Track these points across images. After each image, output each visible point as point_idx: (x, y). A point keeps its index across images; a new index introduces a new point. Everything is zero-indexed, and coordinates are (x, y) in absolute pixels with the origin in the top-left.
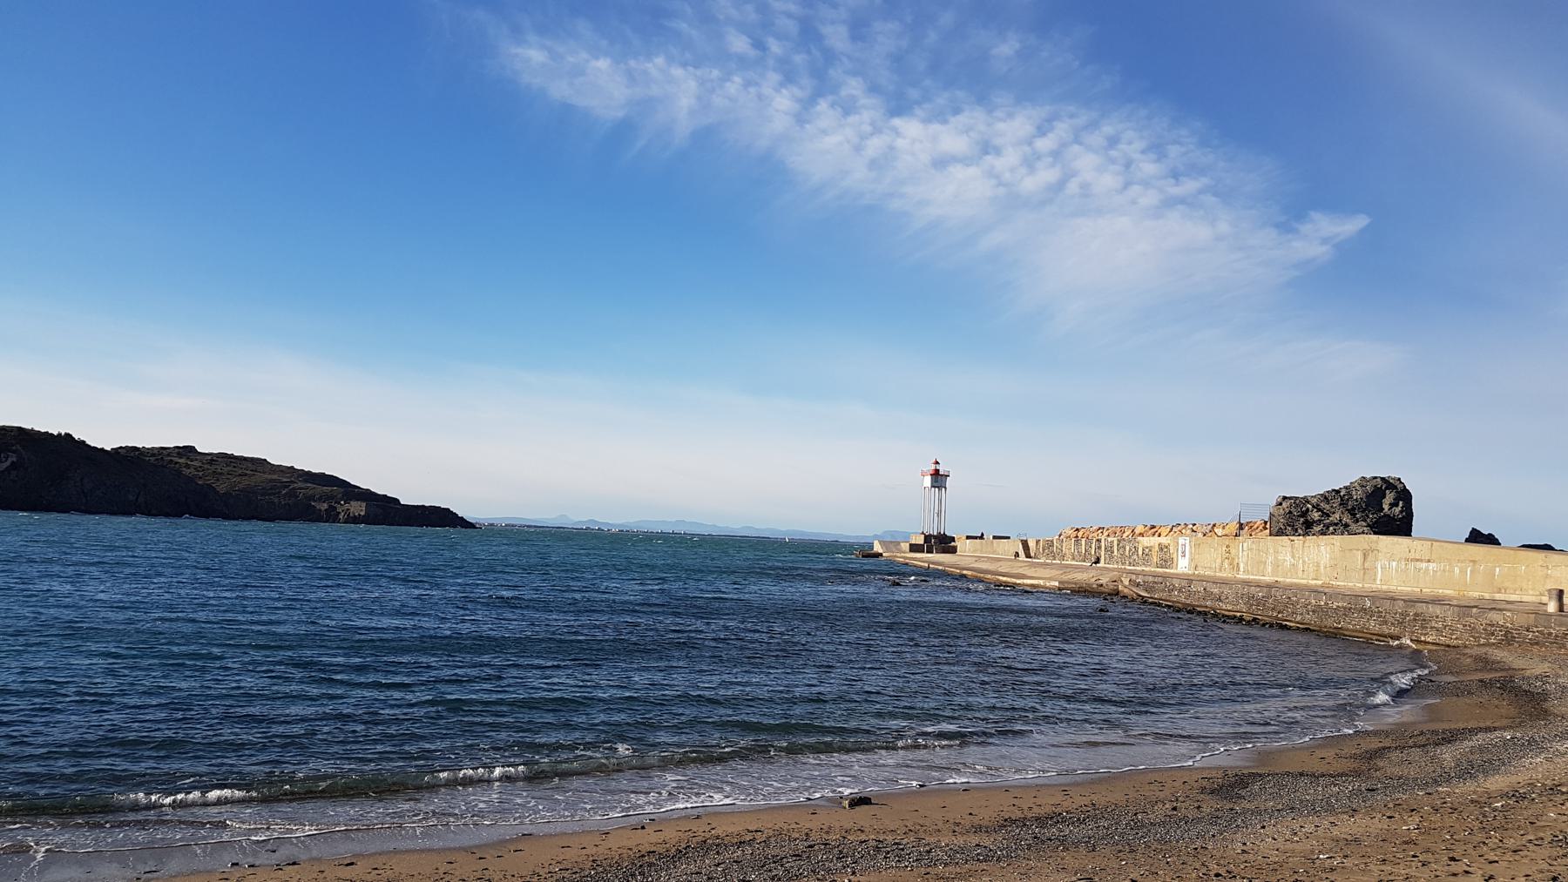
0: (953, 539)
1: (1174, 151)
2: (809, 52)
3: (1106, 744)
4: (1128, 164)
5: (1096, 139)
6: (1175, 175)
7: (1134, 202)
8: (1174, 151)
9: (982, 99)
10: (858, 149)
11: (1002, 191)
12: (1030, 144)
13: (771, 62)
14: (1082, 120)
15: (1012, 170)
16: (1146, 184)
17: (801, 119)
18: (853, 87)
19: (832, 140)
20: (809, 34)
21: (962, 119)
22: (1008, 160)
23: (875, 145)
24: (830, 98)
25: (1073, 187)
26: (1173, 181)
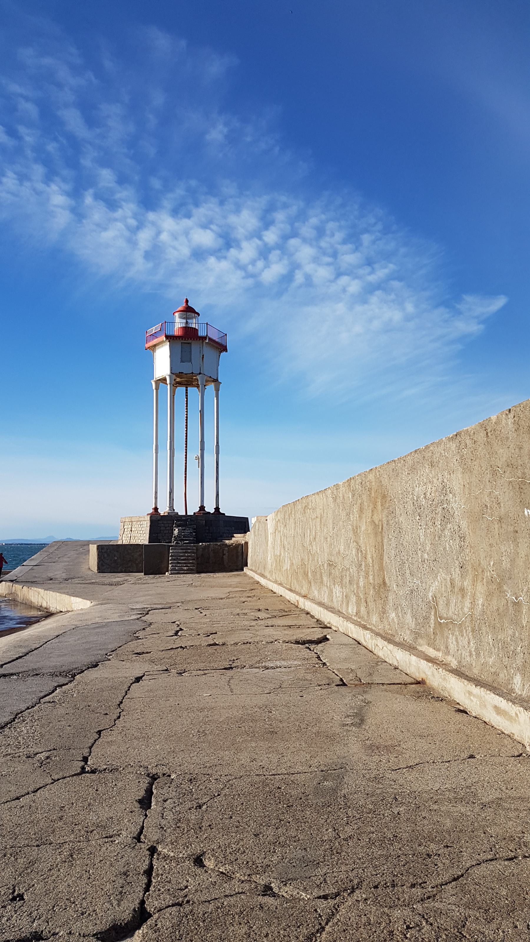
1: (366, 238)
2: (55, 139)
4: (335, 255)
5: (306, 230)
6: (369, 262)
7: (344, 290)
8: (366, 238)
9: (212, 190)
10: (132, 243)
11: (250, 282)
12: (260, 238)
13: (29, 153)
14: (294, 210)
15: (253, 262)
16: (350, 272)
17: (78, 214)
18: (106, 177)
19: (107, 235)
20: (49, 121)
21: (200, 213)
22: (247, 252)
23: (144, 237)
24: (91, 191)
25: (299, 278)
26: (368, 269)
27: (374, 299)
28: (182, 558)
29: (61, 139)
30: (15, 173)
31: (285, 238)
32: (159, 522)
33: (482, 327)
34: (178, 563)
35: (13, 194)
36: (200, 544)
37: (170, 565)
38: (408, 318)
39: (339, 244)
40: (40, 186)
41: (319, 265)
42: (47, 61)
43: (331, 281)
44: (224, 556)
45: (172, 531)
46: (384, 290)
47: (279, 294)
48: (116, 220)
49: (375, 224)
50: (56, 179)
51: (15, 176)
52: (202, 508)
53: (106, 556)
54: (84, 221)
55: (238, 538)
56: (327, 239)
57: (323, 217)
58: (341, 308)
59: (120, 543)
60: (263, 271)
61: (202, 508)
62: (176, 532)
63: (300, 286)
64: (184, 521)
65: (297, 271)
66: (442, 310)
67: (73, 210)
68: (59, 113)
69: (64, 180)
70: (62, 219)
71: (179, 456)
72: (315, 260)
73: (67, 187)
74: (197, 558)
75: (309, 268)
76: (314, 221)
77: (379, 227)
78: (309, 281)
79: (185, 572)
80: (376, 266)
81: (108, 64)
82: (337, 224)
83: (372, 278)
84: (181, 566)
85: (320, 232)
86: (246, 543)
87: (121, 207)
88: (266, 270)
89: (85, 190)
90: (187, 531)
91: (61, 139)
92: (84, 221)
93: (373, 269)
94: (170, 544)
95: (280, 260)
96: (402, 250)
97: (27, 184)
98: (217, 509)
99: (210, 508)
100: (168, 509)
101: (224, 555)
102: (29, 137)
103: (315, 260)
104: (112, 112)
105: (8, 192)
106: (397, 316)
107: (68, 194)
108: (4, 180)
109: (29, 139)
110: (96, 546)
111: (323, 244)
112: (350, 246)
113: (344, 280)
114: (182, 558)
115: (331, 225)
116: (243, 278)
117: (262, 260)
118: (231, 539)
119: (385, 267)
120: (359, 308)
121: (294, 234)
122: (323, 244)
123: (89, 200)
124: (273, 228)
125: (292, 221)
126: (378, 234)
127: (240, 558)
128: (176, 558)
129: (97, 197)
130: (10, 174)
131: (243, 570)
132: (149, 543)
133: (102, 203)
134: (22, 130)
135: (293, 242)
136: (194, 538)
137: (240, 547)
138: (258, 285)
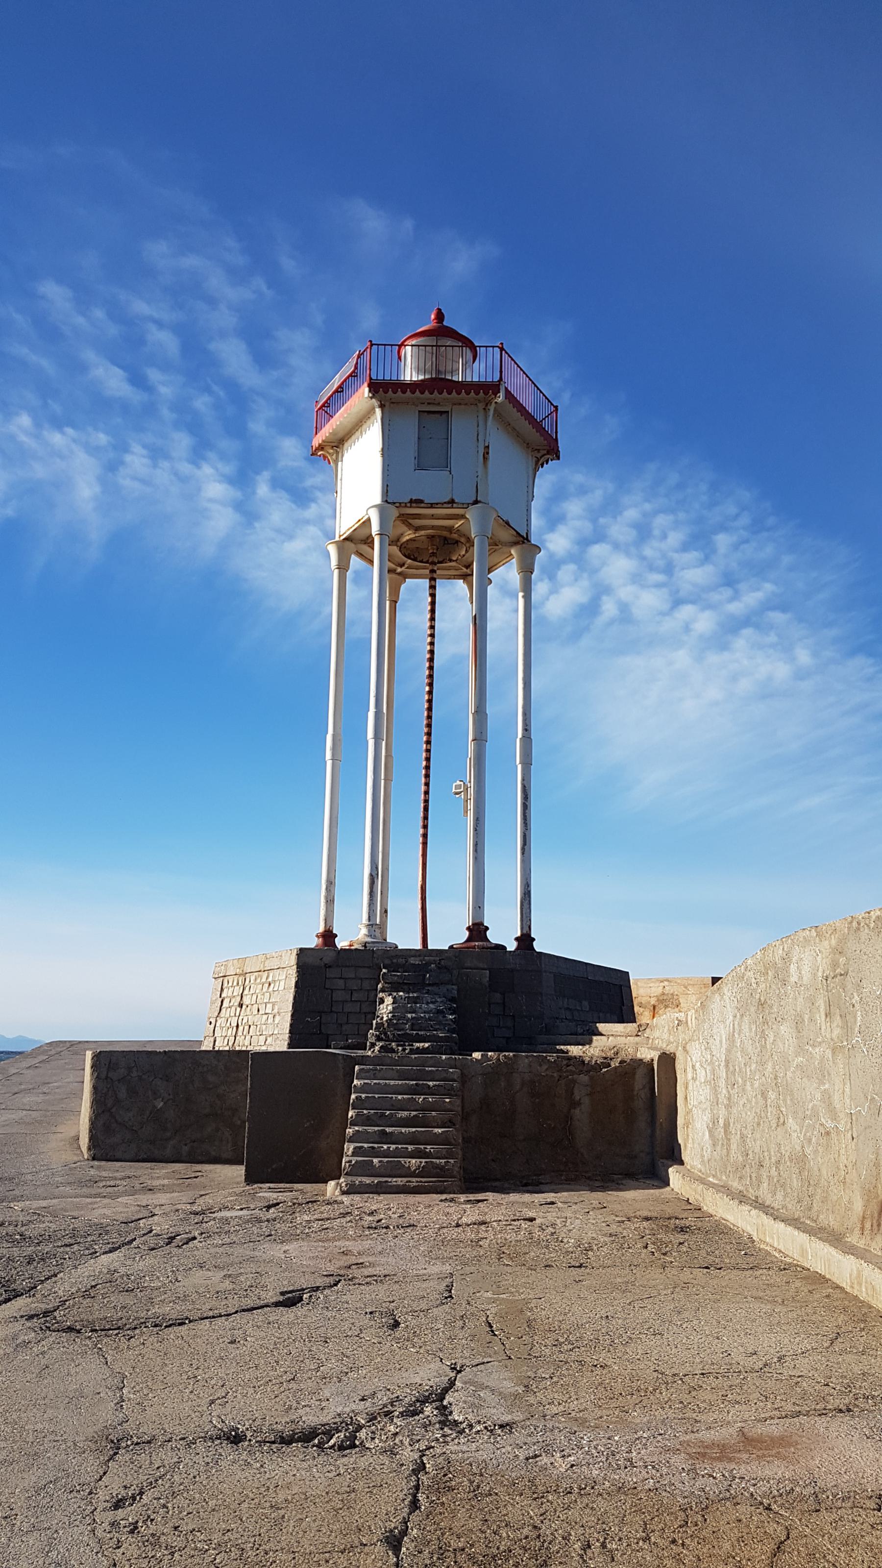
0: (608, 994)
1: (722, 540)
2: (208, 390)
3: (501, 372)
4: (669, 569)
5: (620, 529)
6: (729, 581)
7: (687, 628)
8: (722, 540)
13: (166, 414)
14: (597, 497)
16: (697, 598)
17: (248, 512)
19: (295, 547)
20: (197, 361)
24: (266, 475)
25: (609, 607)
26: (728, 592)
27: (740, 642)
28: (404, 1114)
29: (215, 388)
30: (145, 447)
31: (584, 543)
32: (331, 973)
34: (384, 1137)
35: (143, 481)
36: (477, 1055)
37: (349, 1148)
38: (801, 675)
39: (677, 551)
40: (185, 468)
41: (643, 586)
42: (190, 261)
43: (663, 614)
44: (577, 1111)
45: (374, 1003)
46: (757, 626)
47: (576, 636)
48: (307, 522)
49: (737, 516)
50: (211, 455)
51: (144, 452)
52: (478, 930)
53: (123, 1094)
54: (257, 525)
55: (611, 1040)
56: (655, 544)
57: (647, 507)
58: (682, 658)
59: (207, 1046)
60: (547, 599)
61: (478, 930)
62: (386, 1008)
63: (611, 622)
64: (417, 971)
65: (605, 598)
66: (860, 661)
67: (239, 506)
68: (212, 346)
69: (223, 456)
70: (222, 521)
72: (636, 579)
73: (228, 469)
74: (465, 1117)
75: (626, 592)
76: (631, 514)
77: (745, 520)
78: (625, 615)
79: (414, 1181)
80: (742, 586)
81: (288, 264)
82: (671, 518)
83: (735, 608)
84: (397, 1154)
85: (643, 532)
86: (668, 1060)
87: (314, 500)
88: (552, 598)
89: (258, 473)
90: (426, 1008)
91: (215, 388)
92: (257, 525)
93: (736, 592)
94: (360, 1052)
95: (576, 580)
96: (787, 559)
97: (166, 464)
98: (525, 940)
99: (503, 933)
100: (364, 931)
101: (575, 1104)
102: (166, 387)
103: (636, 579)
104: (296, 342)
105: (134, 478)
106: (782, 671)
107: (231, 481)
108: (128, 458)
109: (165, 391)
111: (648, 552)
112: (693, 555)
113: (687, 611)
114: (404, 1114)
115: (661, 521)
117: (546, 581)
118: (590, 1042)
119: (758, 589)
120: (714, 658)
121: (599, 537)
122: (648, 552)
123: (263, 490)
124: (562, 529)
125: (594, 514)
126: (744, 534)
127: (642, 1123)
128: (378, 1113)
129: (277, 484)
130: (137, 448)
131: (665, 1182)
132: (290, 1046)
133: (284, 494)
134: (154, 375)
135: (597, 550)
136: (452, 1031)
137: (640, 1072)
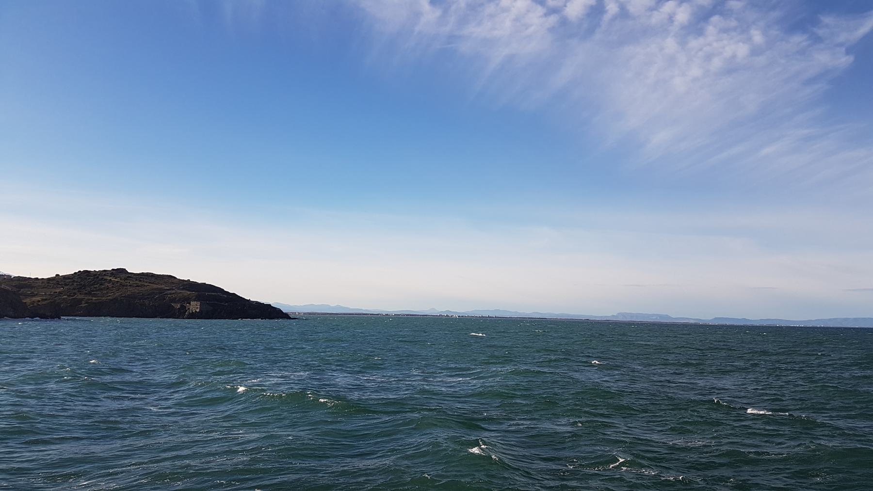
7: (671, 18)
11: (553, 19)
33: (851, 59)
38: (755, 52)
46: (721, 14)
47: (590, 32)
63: (615, 18)
71: (391, 424)
106: (742, 50)
110: (844, 49)
116: (546, 15)
120: (694, 43)
138: (564, 22)
